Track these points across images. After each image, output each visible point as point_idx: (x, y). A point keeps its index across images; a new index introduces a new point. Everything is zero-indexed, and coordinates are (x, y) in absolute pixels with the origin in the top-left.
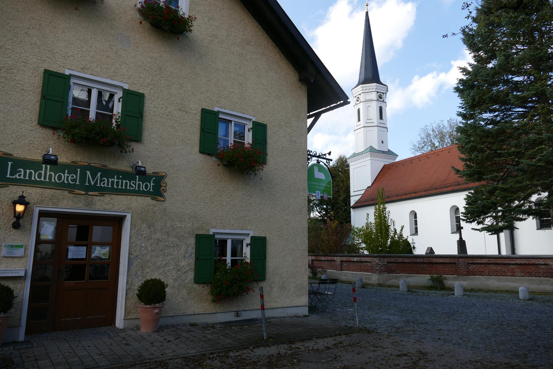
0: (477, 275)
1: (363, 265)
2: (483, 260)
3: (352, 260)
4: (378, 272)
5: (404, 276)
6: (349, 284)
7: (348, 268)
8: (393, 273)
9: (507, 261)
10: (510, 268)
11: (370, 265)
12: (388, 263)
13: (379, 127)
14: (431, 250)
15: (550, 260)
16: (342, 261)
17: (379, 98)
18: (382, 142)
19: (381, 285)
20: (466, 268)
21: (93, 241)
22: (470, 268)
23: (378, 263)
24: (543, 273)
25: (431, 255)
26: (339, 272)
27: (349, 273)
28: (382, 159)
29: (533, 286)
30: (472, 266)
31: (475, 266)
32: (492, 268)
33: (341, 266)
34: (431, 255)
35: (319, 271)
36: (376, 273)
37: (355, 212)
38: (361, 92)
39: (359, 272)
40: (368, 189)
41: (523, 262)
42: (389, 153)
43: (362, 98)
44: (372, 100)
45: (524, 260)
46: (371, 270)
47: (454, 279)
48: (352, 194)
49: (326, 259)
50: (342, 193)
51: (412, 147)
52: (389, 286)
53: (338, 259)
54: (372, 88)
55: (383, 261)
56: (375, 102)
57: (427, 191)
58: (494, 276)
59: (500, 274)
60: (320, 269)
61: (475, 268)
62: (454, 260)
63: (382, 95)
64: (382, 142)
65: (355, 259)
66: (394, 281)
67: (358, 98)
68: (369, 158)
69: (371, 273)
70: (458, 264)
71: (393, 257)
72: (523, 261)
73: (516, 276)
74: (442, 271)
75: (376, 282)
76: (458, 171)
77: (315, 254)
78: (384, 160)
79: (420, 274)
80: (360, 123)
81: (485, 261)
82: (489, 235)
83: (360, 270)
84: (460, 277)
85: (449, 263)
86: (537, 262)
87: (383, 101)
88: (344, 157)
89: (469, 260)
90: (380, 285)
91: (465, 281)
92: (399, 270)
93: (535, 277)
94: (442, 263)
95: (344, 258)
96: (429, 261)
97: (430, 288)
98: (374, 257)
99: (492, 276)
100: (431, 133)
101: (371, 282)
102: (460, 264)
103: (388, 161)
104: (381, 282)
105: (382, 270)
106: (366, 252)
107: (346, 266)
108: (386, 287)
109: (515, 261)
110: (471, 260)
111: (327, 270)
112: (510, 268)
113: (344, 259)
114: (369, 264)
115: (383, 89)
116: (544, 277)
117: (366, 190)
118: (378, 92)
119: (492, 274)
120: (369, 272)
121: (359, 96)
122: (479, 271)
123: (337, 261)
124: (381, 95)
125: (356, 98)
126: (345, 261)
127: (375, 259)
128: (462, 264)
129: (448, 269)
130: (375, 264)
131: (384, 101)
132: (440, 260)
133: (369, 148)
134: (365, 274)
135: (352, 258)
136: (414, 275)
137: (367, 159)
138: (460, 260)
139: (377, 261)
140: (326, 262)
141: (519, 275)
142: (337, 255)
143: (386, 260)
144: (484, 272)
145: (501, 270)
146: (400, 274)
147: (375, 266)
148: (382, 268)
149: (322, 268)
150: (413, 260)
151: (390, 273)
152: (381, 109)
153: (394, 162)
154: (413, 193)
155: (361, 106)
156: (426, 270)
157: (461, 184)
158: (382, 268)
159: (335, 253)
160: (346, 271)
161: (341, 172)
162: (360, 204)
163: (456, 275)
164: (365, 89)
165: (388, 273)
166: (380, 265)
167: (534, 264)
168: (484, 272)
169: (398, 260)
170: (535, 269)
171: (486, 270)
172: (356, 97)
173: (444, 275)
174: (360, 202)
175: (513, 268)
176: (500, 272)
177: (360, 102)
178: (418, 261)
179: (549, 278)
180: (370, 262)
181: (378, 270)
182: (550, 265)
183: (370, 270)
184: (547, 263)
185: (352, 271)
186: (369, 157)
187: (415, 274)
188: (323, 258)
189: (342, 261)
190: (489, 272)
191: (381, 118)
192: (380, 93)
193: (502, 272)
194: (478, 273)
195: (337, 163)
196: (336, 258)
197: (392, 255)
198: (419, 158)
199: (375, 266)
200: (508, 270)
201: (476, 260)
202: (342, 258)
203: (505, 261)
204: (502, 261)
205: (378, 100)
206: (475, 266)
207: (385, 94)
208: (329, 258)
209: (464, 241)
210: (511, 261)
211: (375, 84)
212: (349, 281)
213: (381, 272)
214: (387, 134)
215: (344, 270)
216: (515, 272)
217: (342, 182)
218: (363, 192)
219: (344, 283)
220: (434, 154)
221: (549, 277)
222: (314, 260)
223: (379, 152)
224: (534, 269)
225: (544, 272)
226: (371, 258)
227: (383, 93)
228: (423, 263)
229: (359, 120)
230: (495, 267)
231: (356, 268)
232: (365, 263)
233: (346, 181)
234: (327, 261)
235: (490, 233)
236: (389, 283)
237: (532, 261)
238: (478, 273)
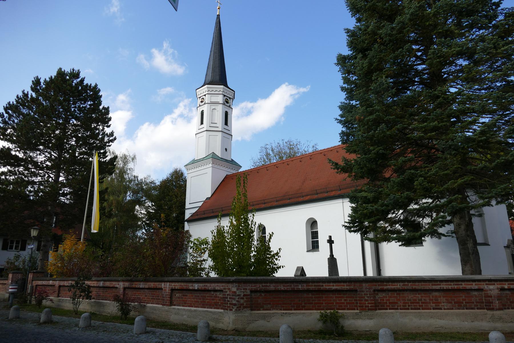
0: (387, 309)
1: (208, 296)
2: (396, 284)
3: (191, 288)
4: (235, 308)
5: (277, 313)
6: (183, 330)
7: (183, 301)
8: (259, 310)
9: (429, 285)
10: (433, 297)
11: (221, 296)
12: (252, 291)
13: (223, 133)
14: (301, 271)
15: (485, 283)
16: (172, 290)
17: (225, 103)
18: (226, 149)
19: (239, 331)
20: (372, 298)
22: (377, 297)
23: (235, 292)
24: (476, 303)
25: (301, 278)
26: (166, 308)
27: (184, 309)
29: (466, 323)
30: (381, 295)
31: (384, 295)
32: (408, 297)
33: (171, 297)
34: (301, 278)
35: (134, 307)
36: (231, 310)
37: (190, 226)
38: (207, 93)
39: (201, 307)
40: (207, 201)
41: (450, 286)
42: (232, 162)
43: (207, 99)
44: (217, 103)
45: (452, 283)
46: (224, 305)
47: (357, 317)
48: (187, 206)
49: (147, 286)
50: (174, 209)
51: (253, 164)
52: (254, 333)
53: (166, 286)
54: (218, 90)
55: (244, 289)
56: (221, 105)
57: (278, 201)
58: (412, 309)
59: (419, 306)
60: (136, 303)
61: (384, 297)
62: (355, 286)
63: (229, 100)
64: (226, 149)
65: (196, 286)
66: (261, 324)
67: (203, 99)
68: (210, 165)
69: (222, 311)
70: (360, 291)
71: (261, 282)
72: (451, 285)
73: (441, 309)
74: (337, 303)
75: (231, 327)
76: (337, 164)
77: (129, 278)
78: (227, 169)
79: (313, 310)
80: (202, 126)
81: (399, 286)
82: (400, 246)
83: (203, 305)
84: (363, 313)
85: (347, 291)
86: (468, 287)
88: (180, 171)
89: (376, 285)
90: (237, 332)
91: (371, 319)
92: (270, 304)
93: (467, 309)
94: (336, 291)
95: (177, 284)
96: (317, 288)
97: (322, 334)
98: (229, 282)
99: (408, 309)
100: (271, 153)
101: (220, 326)
102: (363, 291)
104: (239, 326)
105: (243, 304)
106: (213, 275)
107: (179, 298)
108: (248, 335)
109: (440, 285)
110: (379, 285)
111: (148, 305)
112: (433, 297)
113: (177, 286)
114: (220, 294)
115: (230, 94)
116: (478, 309)
117: (205, 202)
118: (224, 96)
119: (409, 306)
120: (218, 308)
122: (390, 303)
123: (165, 290)
124: (228, 100)
125: (201, 99)
126: (177, 290)
127: (230, 286)
128: (367, 291)
129: (345, 300)
130: (231, 294)
131: (230, 106)
132: (333, 286)
133: (212, 154)
134: (211, 312)
135: (190, 284)
136: (293, 311)
137: (208, 166)
138: (364, 285)
139: (234, 289)
140: (146, 290)
141: (446, 307)
142: (166, 279)
143: (249, 287)
144: (397, 303)
145: (421, 300)
146: (270, 310)
147: (230, 298)
148: (242, 301)
149: (139, 301)
150: (272, 287)
151: (254, 310)
152: (226, 114)
153: (238, 172)
154: (263, 203)
155: (205, 108)
156: (312, 303)
157: (319, 193)
158: (242, 301)
159: (162, 276)
160: (179, 306)
161: (175, 186)
162: (196, 217)
163: (357, 309)
164: (211, 90)
165: (252, 310)
166: (239, 295)
167: (465, 290)
168: (397, 303)
169: (268, 286)
170: (465, 297)
171: (399, 300)
172: (200, 97)
173: (340, 311)
174: (197, 215)
175: (436, 297)
176: (418, 303)
177: (205, 104)
178: (300, 287)
179: (486, 311)
180: (221, 291)
181: (235, 305)
182: (486, 291)
183: (220, 305)
184: (482, 287)
185: (189, 306)
186: (211, 164)
187: (295, 310)
188: (142, 285)
189: (172, 290)
190: (404, 303)
191: (226, 123)
193: (422, 303)
194: (389, 306)
195: (172, 177)
196: (163, 284)
197: (259, 278)
199: (230, 298)
200: (430, 300)
201: (386, 285)
202: (173, 284)
203: (426, 285)
204: (422, 285)
205: (224, 104)
206: (384, 295)
207: (231, 100)
208: (152, 285)
209: (335, 259)
210: (435, 285)
211: (222, 86)
212: (183, 324)
213: (240, 308)
215: (175, 305)
216: (440, 303)
217: (176, 197)
218: (200, 204)
219: (175, 329)
220: (283, 163)
221: (484, 309)
222: (128, 288)
223: (222, 159)
224: (464, 298)
225: (478, 301)
226: (224, 284)
227: (230, 98)
228: (308, 291)
229: (202, 123)
230: (412, 296)
231: (197, 302)
232: (212, 293)
233: (180, 196)
234: (149, 289)
235: (400, 243)
236: (252, 327)
237: (462, 285)
238: (389, 306)
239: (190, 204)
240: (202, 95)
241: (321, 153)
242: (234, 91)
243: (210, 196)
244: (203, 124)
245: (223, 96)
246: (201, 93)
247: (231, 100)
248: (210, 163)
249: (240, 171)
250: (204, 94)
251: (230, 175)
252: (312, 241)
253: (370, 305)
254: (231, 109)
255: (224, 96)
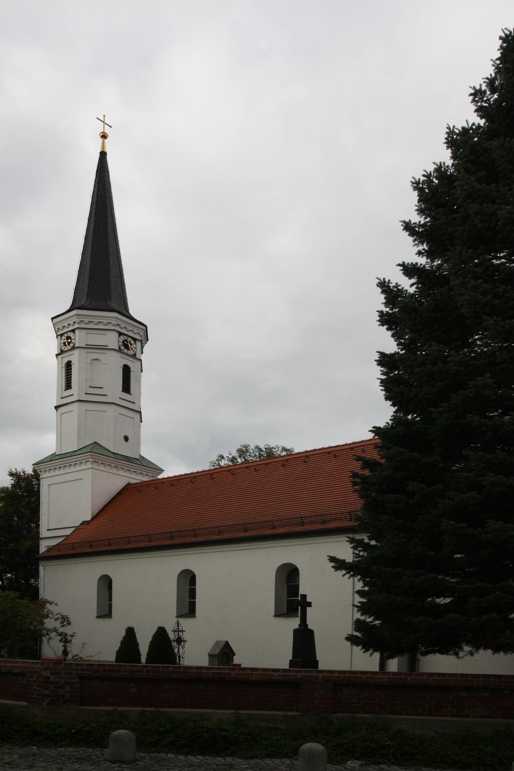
17: (123, 348)
21: (377, 669)
28: (83, 467)
38: (77, 326)
43: (79, 339)
44: (104, 348)
48: (44, 533)
63: (132, 342)
67: (68, 338)
73: (467, 716)
78: (127, 474)
80: (69, 392)
87: (134, 356)
103: (136, 478)
117: (77, 528)
118: (120, 334)
121: (71, 334)
125: (63, 338)
131: (135, 355)
155: (75, 357)
163: (297, 711)
177: (74, 348)
191: (126, 387)
192: (126, 338)
198: (212, 474)
205: (120, 351)
207: (139, 344)
209: (312, 632)
214: (140, 426)
218: (68, 532)
220: (247, 468)
227: (135, 340)
229: (68, 386)
239: (48, 530)
240: (66, 330)
241: (329, 453)
242: (146, 327)
243: (88, 518)
244: (71, 388)
245: (117, 335)
246: (69, 325)
247: (139, 344)
248: (89, 461)
249: (160, 477)
250: (71, 328)
251: (136, 483)
252: (287, 599)
253: (322, 706)
254: (138, 363)
255: (120, 334)
